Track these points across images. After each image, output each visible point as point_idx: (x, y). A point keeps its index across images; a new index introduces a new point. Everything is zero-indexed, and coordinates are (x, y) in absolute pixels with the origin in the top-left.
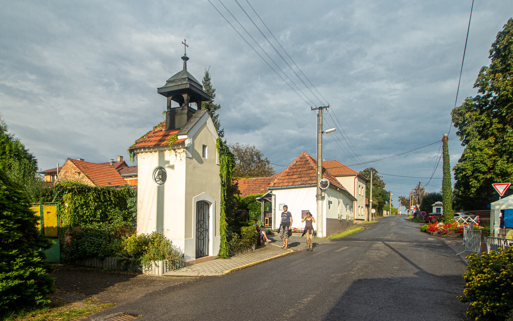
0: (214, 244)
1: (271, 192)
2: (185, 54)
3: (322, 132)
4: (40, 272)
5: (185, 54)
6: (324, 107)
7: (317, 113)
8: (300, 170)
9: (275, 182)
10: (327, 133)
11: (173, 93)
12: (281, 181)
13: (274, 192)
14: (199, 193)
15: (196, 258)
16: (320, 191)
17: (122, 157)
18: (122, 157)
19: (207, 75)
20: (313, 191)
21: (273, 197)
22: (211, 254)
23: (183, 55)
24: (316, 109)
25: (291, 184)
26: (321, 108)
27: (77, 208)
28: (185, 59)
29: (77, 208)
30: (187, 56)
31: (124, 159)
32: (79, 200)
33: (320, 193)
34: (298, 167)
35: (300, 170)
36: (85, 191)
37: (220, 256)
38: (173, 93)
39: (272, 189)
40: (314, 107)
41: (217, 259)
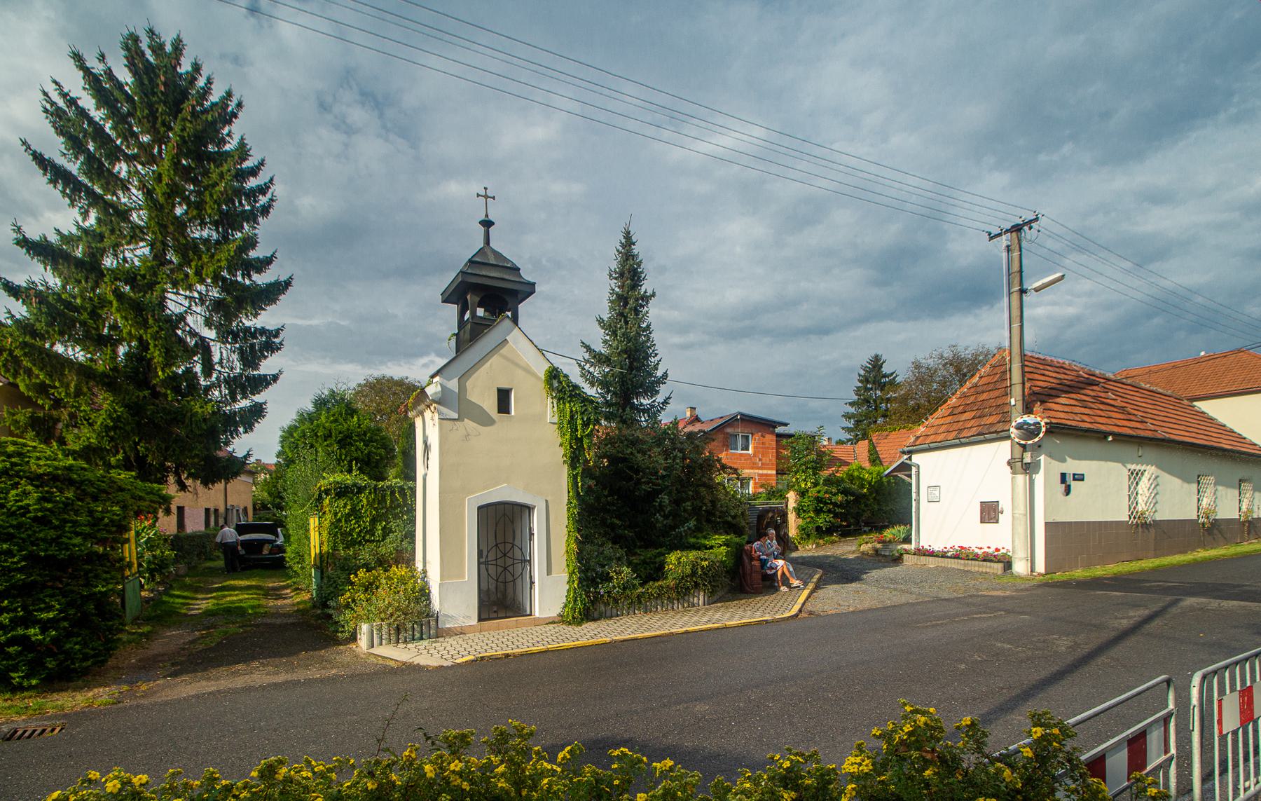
0: (549, 588)
1: (910, 458)
2: (487, 216)
3: (1023, 291)
4: (35, 635)
5: (487, 216)
6: (1025, 224)
7: (1005, 244)
8: (985, 396)
9: (918, 434)
10: (1037, 290)
11: (458, 294)
12: (932, 431)
13: (916, 458)
14: (485, 489)
15: (480, 620)
16: (1018, 450)
17: (693, 409)
18: (693, 409)
19: (627, 235)
20: (1003, 450)
21: (914, 469)
22: (537, 613)
23: (483, 218)
24: (1000, 235)
25: (954, 434)
26: (1017, 229)
27: (340, 520)
28: (487, 224)
29: (340, 520)
30: (491, 218)
31: (697, 412)
32: (344, 506)
33: (1017, 455)
34: (980, 389)
35: (985, 396)
36: (352, 492)
37: (562, 620)
38: (458, 294)
39: (910, 452)
40: (996, 231)
41: (553, 623)
